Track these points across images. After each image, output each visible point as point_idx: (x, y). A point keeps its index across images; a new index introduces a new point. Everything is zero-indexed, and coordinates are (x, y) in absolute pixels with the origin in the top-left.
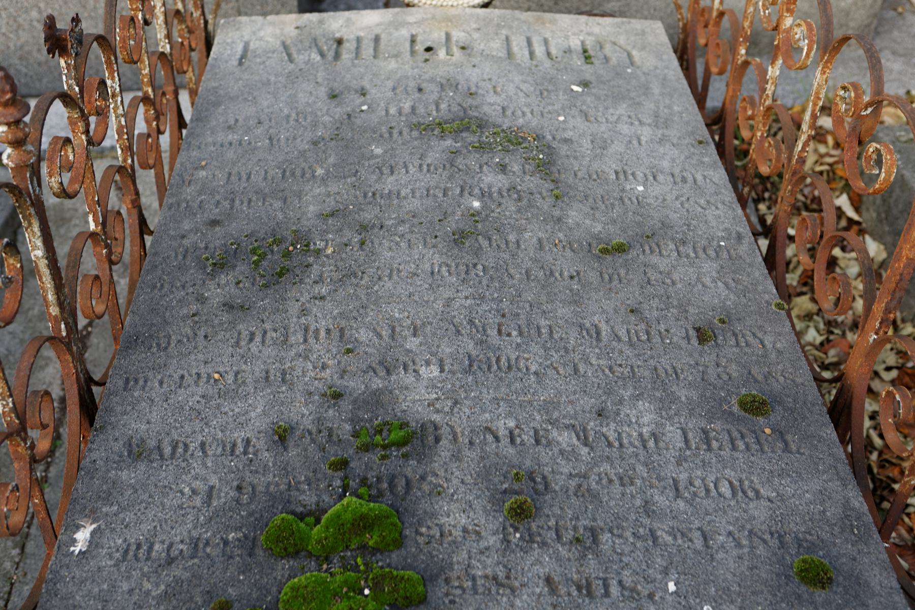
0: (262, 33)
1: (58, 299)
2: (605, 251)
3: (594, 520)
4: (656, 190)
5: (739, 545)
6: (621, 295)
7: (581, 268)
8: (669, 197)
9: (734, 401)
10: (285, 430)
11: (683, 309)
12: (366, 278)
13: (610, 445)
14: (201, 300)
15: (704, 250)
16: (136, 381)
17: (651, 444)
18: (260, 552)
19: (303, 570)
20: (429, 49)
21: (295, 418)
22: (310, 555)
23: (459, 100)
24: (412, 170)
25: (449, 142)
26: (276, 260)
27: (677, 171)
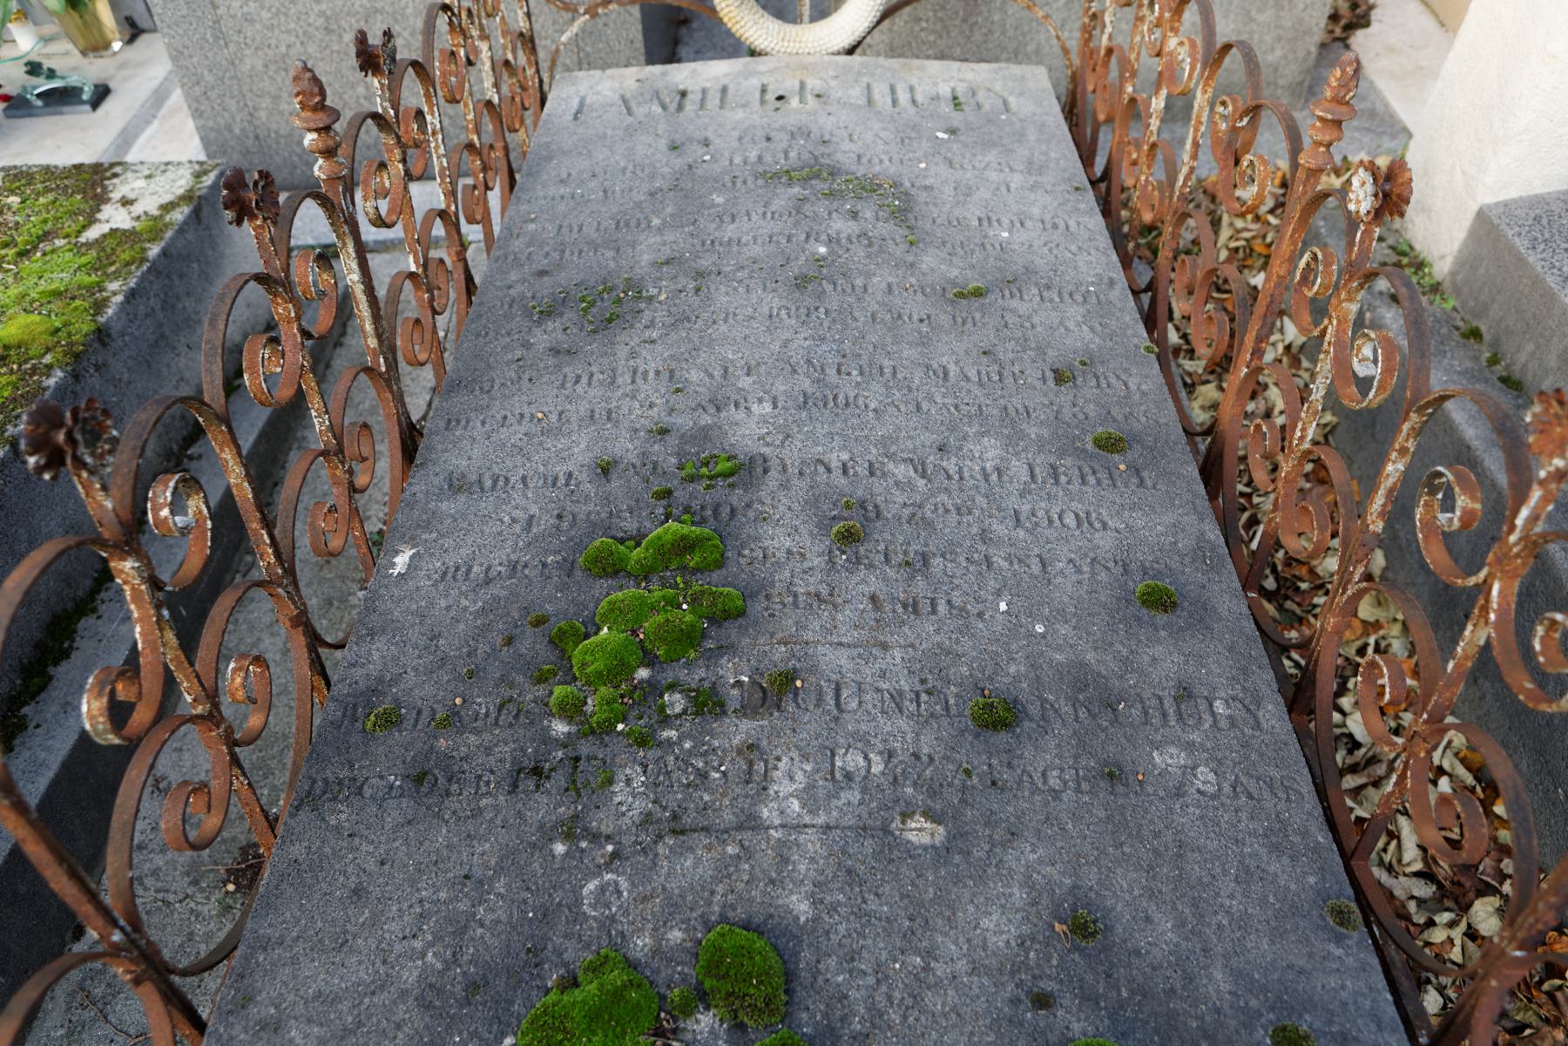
0: (600, 87)
1: (376, 329)
2: (960, 295)
3: (927, 545)
4: (1022, 236)
5: (1079, 571)
6: (975, 338)
7: (932, 312)
8: (1036, 243)
9: (1089, 438)
10: (608, 463)
11: (1041, 351)
12: (700, 322)
13: (949, 477)
14: (527, 345)
15: (1071, 295)
16: (458, 421)
17: (994, 477)
18: (578, 574)
19: (621, 588)
20: (780, 98)
21: (618, 452)
22: (629, 575)
23: (810, 148)
24: (754, 218)
25: (796, 190)
26: (607, 308)
27: (1047, 218)
